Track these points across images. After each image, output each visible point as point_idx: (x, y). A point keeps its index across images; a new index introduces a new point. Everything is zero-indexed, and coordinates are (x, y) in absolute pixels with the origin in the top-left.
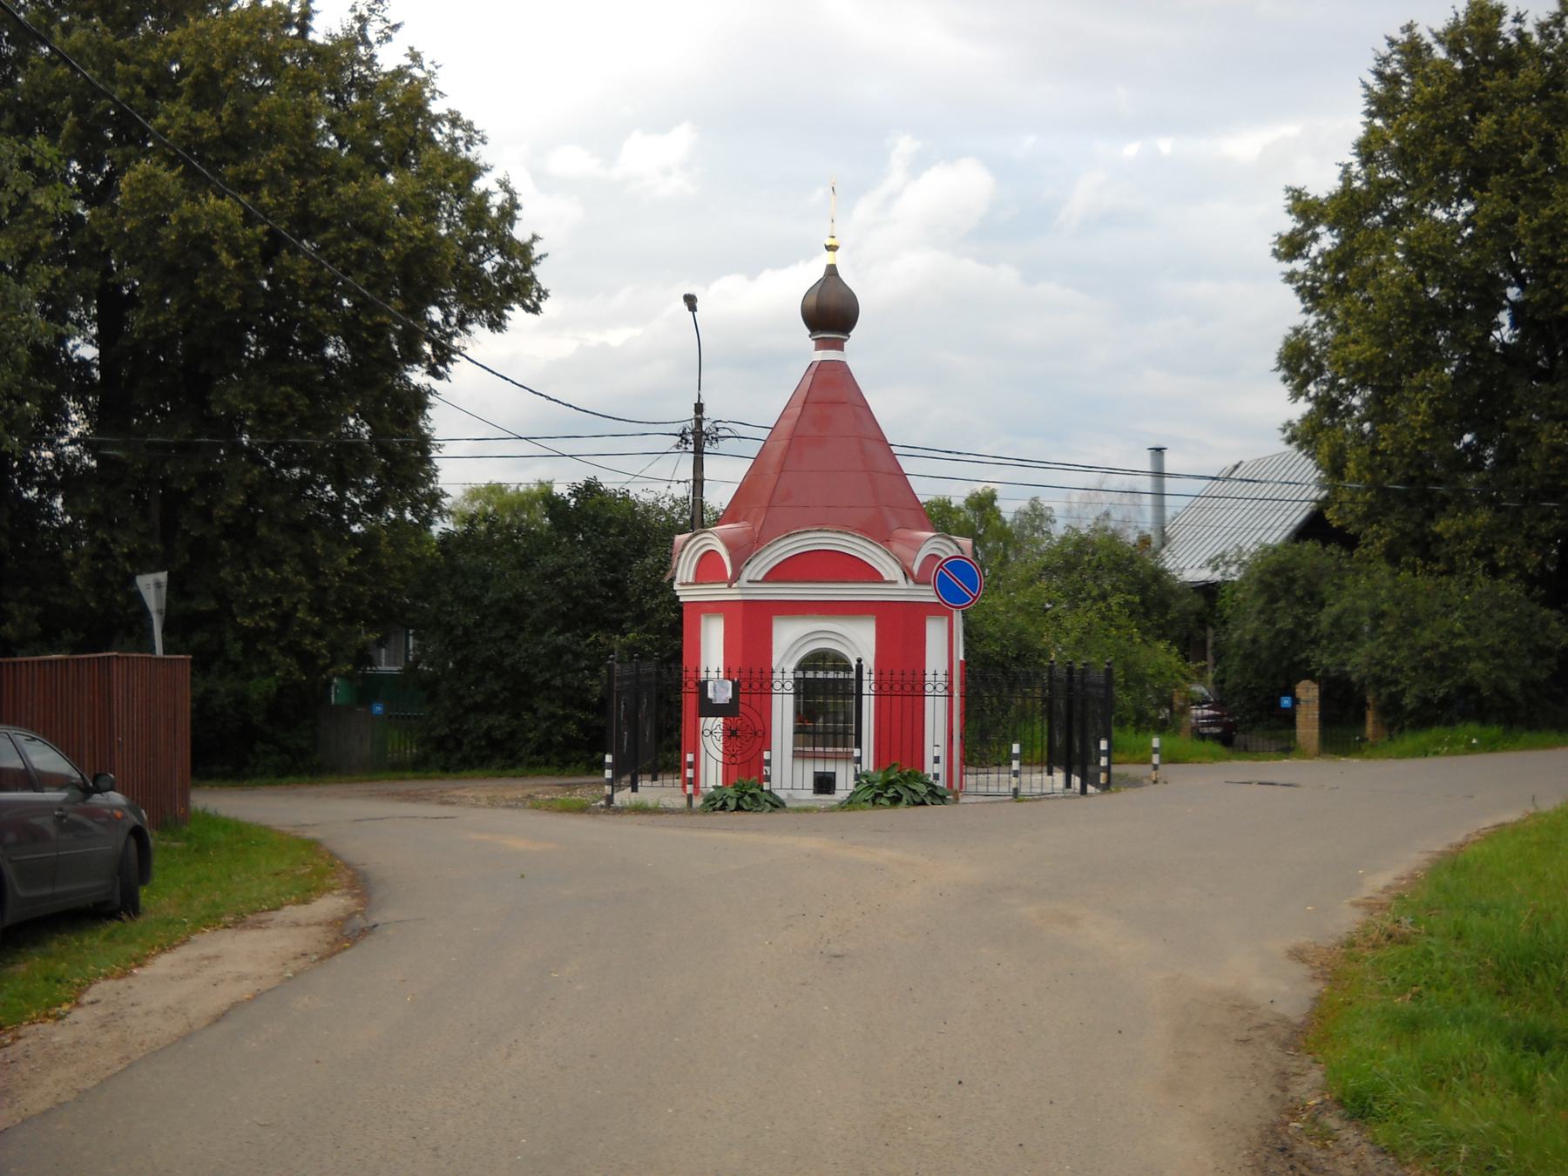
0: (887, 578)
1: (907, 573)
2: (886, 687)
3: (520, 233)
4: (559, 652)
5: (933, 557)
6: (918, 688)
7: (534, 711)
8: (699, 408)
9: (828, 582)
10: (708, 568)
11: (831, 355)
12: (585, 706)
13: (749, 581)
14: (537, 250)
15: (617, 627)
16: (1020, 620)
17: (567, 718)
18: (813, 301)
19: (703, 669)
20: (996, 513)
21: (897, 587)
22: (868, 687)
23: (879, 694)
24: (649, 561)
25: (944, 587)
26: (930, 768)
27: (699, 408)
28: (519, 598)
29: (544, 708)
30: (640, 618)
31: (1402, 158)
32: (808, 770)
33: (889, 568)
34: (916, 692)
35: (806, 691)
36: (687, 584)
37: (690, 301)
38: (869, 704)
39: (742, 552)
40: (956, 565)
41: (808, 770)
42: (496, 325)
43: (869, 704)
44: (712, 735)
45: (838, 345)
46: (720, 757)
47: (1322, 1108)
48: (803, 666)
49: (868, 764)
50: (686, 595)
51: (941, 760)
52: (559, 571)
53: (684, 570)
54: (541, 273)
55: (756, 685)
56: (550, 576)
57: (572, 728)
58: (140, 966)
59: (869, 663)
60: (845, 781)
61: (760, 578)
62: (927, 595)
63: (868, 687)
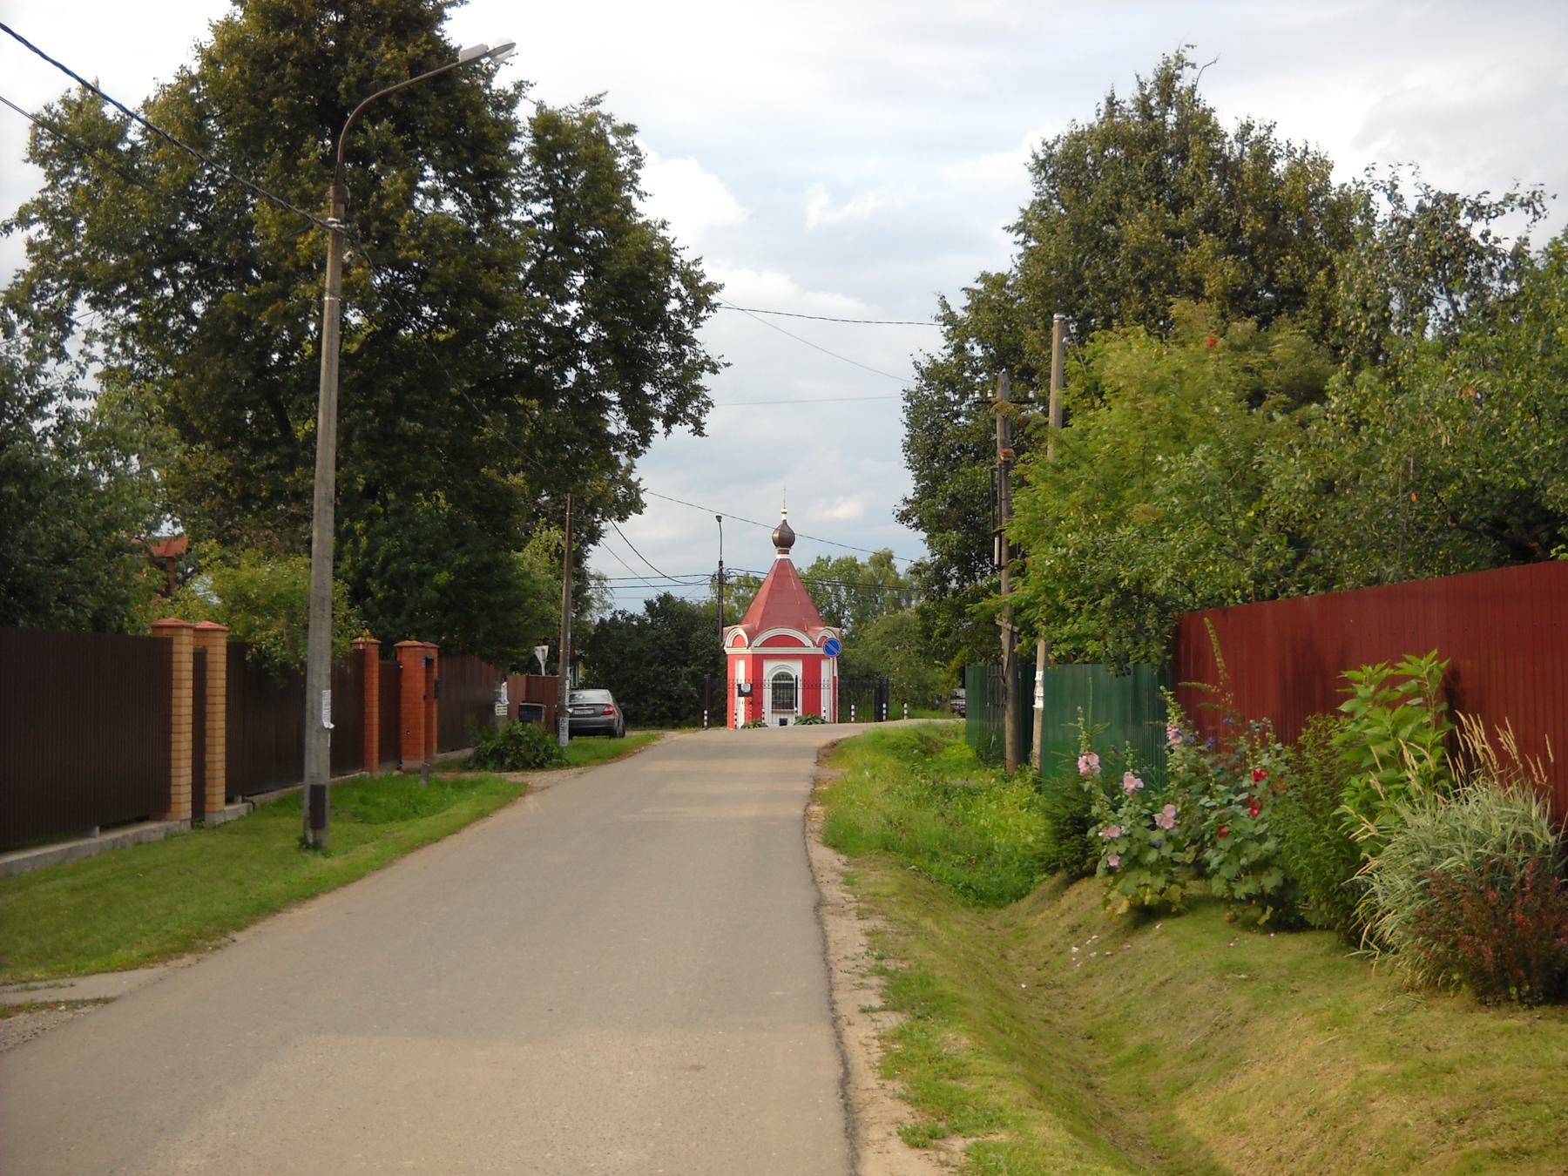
1: (814, 644)
3: (633, 478)
4: (658, 675)
7: (646, 701)
8: (721, 563)
10: (737, 641)
11: (785, 556)
12: (670, 699)
14: (642, 486)
15: (685, 664)
17: (662, 705)
18: (777, 535)
20: (892, 568)
24: (699, 633)
25: (827, 649)
26: (823, 715)
27: (721, 563)
28: (641, 651)
29: (652, 700)
30: (696, 658)
31: (1300, 163)
32: (777, 718)
33: (807, 642)
34: (426, 727)
35: (775, 687)
37: (719, 518)
40: (832, 642)
41: (777, 718)
42: (649, 604)
44: (740, 707)
49: (800, 714)
50: (728, 651)
52: (659, 638)
53: (728, 641)
56: (654, 641)
59: (800, 677)
60: (791, 720)
62: (821, 651)
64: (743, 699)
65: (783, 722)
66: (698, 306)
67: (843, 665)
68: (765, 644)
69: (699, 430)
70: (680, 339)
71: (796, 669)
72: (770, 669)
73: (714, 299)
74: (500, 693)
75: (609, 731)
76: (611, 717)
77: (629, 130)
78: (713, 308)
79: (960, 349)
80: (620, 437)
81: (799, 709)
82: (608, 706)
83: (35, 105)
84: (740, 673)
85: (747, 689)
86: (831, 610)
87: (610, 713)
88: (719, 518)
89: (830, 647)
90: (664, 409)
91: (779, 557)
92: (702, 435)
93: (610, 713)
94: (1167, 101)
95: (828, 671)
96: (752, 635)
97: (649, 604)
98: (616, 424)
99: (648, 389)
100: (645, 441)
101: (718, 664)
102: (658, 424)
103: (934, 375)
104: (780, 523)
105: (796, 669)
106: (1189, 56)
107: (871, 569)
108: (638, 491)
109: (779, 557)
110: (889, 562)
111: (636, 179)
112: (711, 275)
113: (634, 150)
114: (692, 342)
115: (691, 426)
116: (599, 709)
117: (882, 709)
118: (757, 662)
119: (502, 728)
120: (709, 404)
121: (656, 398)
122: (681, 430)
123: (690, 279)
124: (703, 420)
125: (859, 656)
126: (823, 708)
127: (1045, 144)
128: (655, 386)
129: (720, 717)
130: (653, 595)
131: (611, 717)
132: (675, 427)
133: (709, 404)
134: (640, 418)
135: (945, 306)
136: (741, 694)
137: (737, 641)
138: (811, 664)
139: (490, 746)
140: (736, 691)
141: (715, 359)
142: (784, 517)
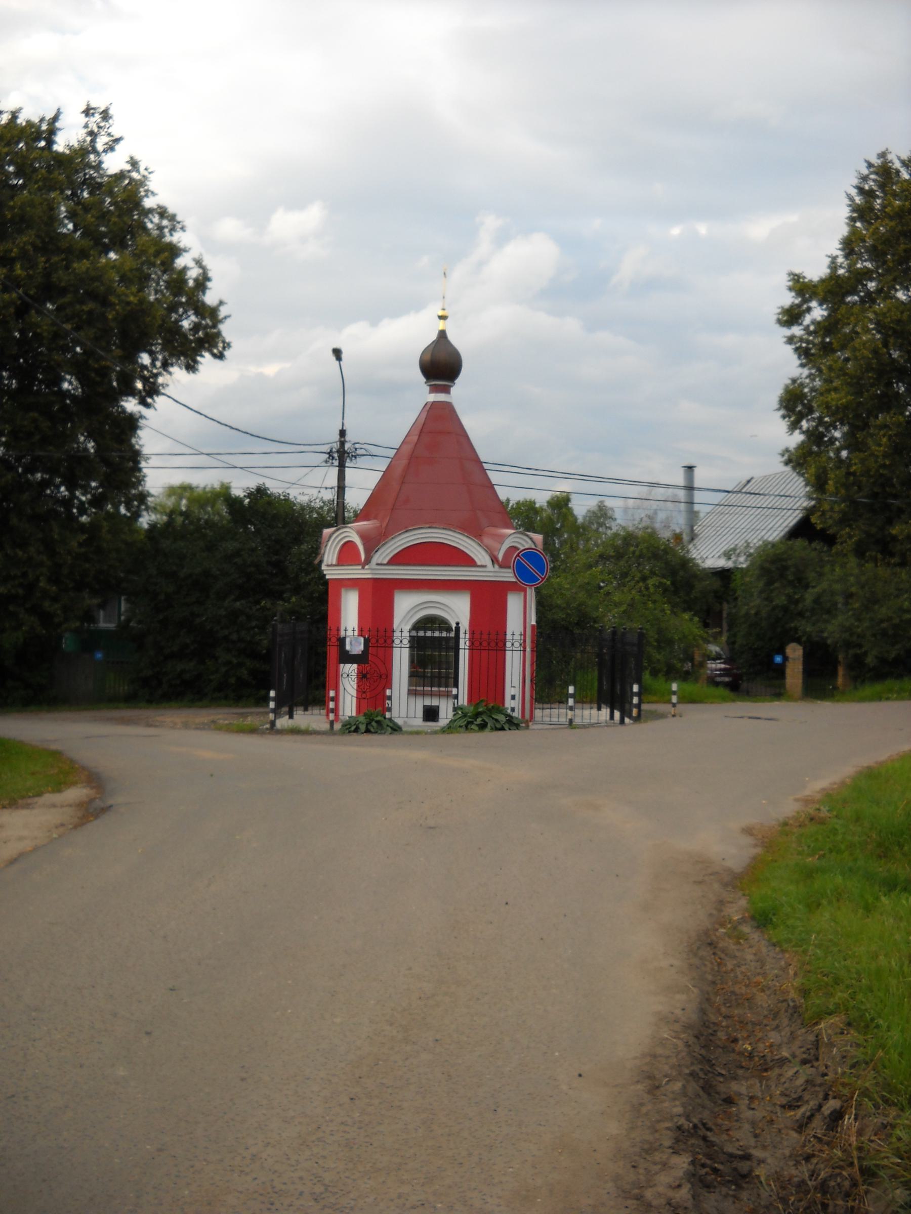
0: (479, 563)
1: (494, 560)
2: (477, 644)
5: (513, 548)
6: (500, 644)
8: (342, 433)
9: (457, 566)
10: (347, 554)
11: (441, 397)
13: (378, 564)
15: (278, 595)
16: (582, 595)
19: (342, 628)
22: (464, 643)
24: (304, 547)
25: (521, 571)
26: (509, 703)
27: (342, 433)
30: (297, 590)
32: (419, 705)
33: (480, 556)
35: (416, 644)
36: (331, 565)
38: (464, 656)
39: (373, 543)
40: (530, 555)
41: (419, 705)
43: (464, 656)
45: (446, 390)
46: (354, 693)
48: (416, 627)
49: (463, 700)
50: (331, 573)
51: (517, 697)
53: (330, 555)
54: (226, 330)
55: (381, 641)
59: (465, 625)
61: (385, 562)
62: (508, 576)
63: (464, 643)
68: (397, 560)
83: (597, 712)
91: (433, 397)
104: (434, 336)
107: (549, 511)
108: (216, 321)
109: (433, 397)
110: (567, 505)
126: (509, 691)
142: (441, 325)
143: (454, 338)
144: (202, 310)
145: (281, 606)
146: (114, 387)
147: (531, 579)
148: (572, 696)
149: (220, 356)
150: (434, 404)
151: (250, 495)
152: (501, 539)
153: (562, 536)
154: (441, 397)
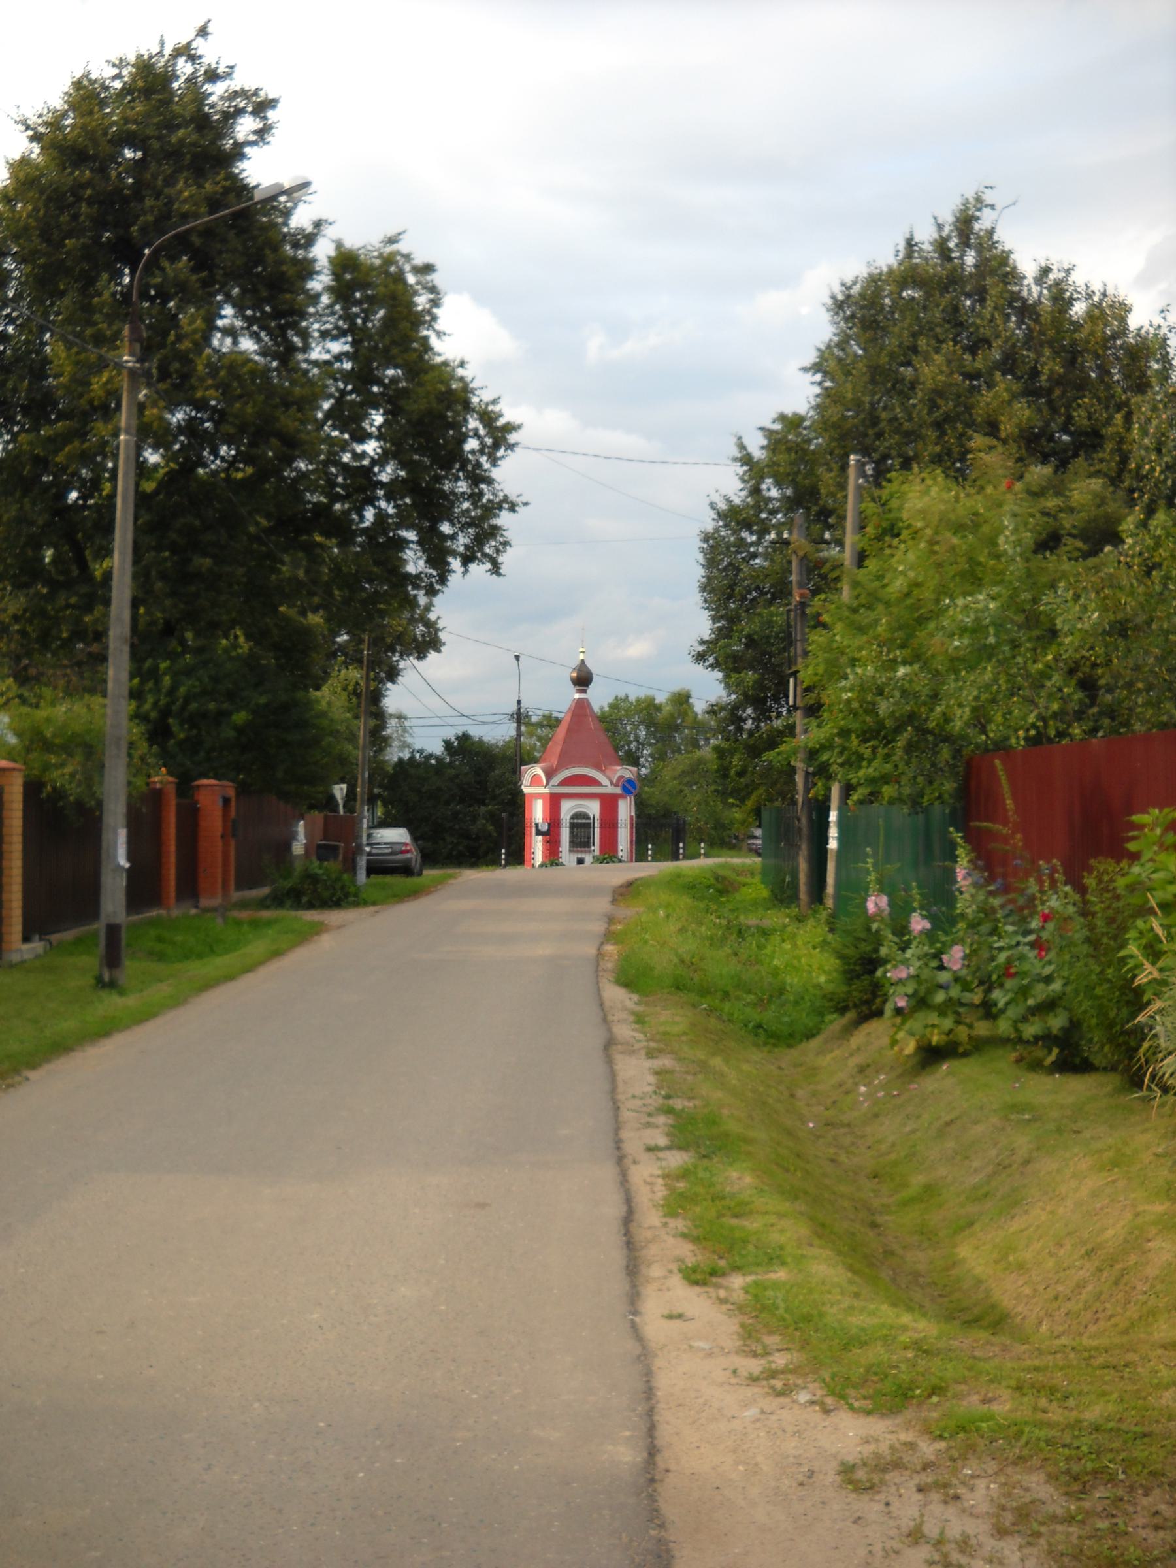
1: (612, 783)
3: (432, 616)
5: (622, 777)
8: (519, 702)
11: (583, 696)
15: (483, 803)
16: (666, 798)
18: (575, 674)
20: (691, 706)
21: (608, 788)
22: (597, 825)
23: (601, 827)
24: (497, 772)
25: (624, 788)
26: (620, 854)
27: (519, 702)
30: (494, 798)
32: (574, 857)
35: (573, 826)
37: (517, 658)
38: (597, 831)
40: (630, 781)
41: (574, 857)
42: (448, 744)
43: (597, 831)
44: (537, 847)
45: (584, 691)
47: (405, 629)
48: (572, 818)
49: (597, 853)
50: (526, 790)
51: (580, 856)
52: (457, 776)
53: (526, 780)
54: (442, 636)
57: (461, 848)
58: (455, 878)
59: (597, 816)
60: (588, 858)
62: (618, 791)
63: (597, 825)
64: (540, 838)
65: (580, 861)
66: (496, 446)
67: (640, 805)
68: (564, 783)
69: (496, 569)
70: (478, 478)
71: (593, 809)
72: (567, 809)
73: (512, 438)
74: (296, 833)
75: (406, 870)
76: (409, 856)
77: (428, 269)
78: (511, 447)
79: (756, 491)
80: (418, 576)
81: (596, 848)
82: (406, 844)
84: (538, 813)
85: (544, 827)
86: (630, 750)
87: (407, 852)
88: (517, 658)
89: (628, 787)
90: (461, 549)
91: (577, 696)
92: (498, 574)
93: (407, 852)
94: (965, 243)
95: (625, 810)
96: (550, 774)
97: (448, 744)
98: (414, 562)
99: (446, 528)
100: (443, 580)
101: (516, 803)
102: (455, 564)
103: (732, 516)
105: (593, 809)
106: (989, 197)
108: (437, 630)
109: (577, 696)
111: (434, 318)
112: (509, 413)
113: (433, 289)
114: (489, 481)
115: (488, 566)
116: (397, 848)
117: (678, 848)
118: (554, 801)
119: (298, 866)
120: (506, 544)
121: (453, 537)
122: (479, 570)
123: (488, 418)
124: (500, 559)
125: (655, 795)
126: (620, 847)
127: (843, 284)
128: (453, 525)
129: (518, 856)
130: (451, 734)
131: (409, 856)
132: (473, 567)
133: (506, 544)
134: (438, 556)
135: (742, 447)
136: (539, 833)
137: (535, 780)
138: (609, 804)
139: (288, 884)
140: (534, 830)
141: (513, 498)
142: (582, 656)
143: (589, 664)
144: (429, 624)
145: (483, 809)
146: (66, 498)
147: (629, 793)
148: (386, 535)
149: (439, 651)
150: (579, 700)
151: (458, 738)
152: (616, 771)
153: (682, 733)
154: (583, 696)
